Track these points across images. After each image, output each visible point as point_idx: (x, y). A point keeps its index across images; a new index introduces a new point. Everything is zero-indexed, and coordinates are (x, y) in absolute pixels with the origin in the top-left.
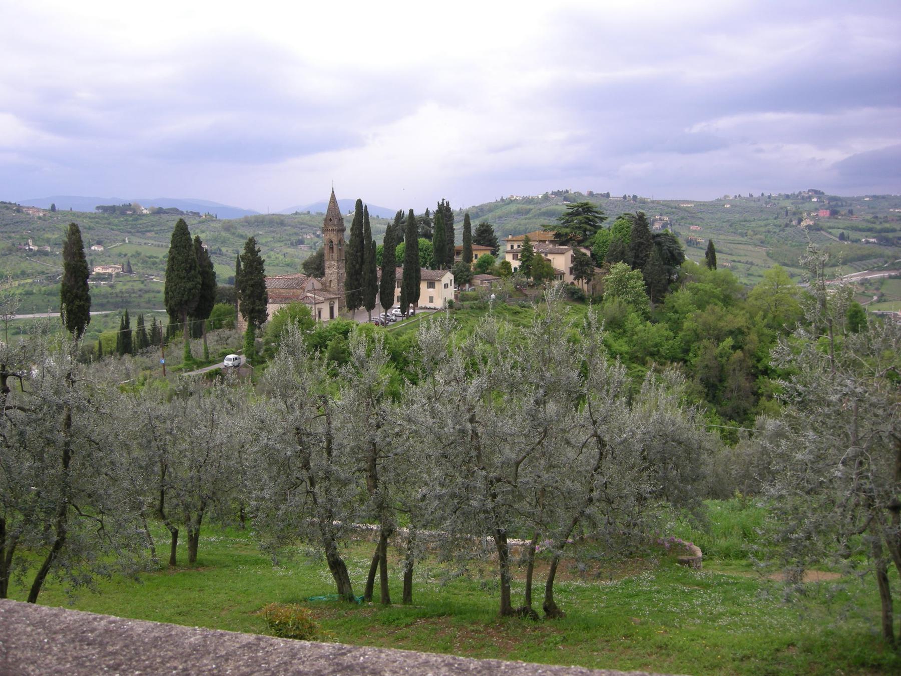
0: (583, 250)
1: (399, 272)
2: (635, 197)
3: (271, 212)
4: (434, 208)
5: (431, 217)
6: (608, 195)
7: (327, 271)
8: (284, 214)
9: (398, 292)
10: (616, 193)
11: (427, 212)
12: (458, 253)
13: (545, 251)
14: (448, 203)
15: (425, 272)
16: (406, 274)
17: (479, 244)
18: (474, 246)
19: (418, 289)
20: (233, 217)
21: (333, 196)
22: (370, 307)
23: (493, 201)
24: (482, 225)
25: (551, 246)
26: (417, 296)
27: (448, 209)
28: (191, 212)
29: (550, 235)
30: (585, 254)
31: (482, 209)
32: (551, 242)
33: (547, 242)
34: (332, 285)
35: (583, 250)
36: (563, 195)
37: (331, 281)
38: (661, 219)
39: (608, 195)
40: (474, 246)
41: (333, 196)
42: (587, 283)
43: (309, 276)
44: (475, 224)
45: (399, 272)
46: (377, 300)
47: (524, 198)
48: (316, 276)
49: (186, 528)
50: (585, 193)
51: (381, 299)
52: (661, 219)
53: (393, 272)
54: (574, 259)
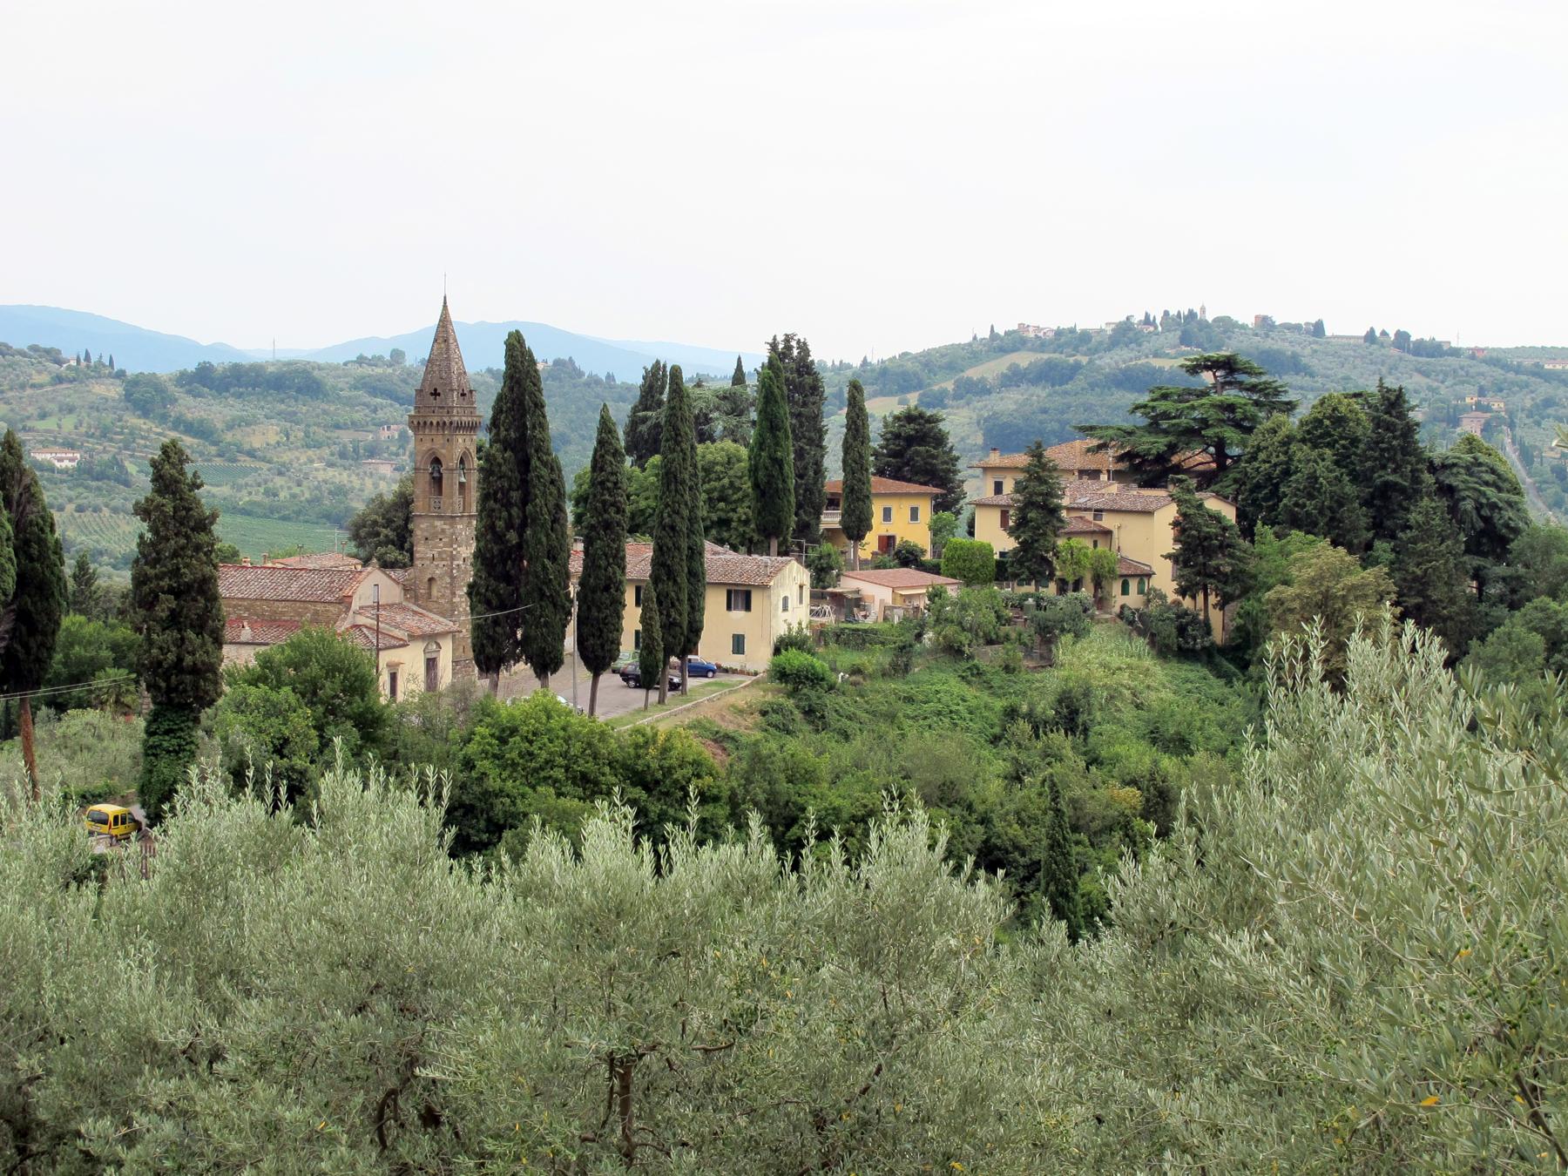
0: (1213, 504)
1: (639, 556)
2: (1402, 337)
3: (285, 357)
4: (756, 358)
5: (752, 381)
6: (1318, 329)
7: (421, 550)
8: (321, 361)
9: (632, 618)
10: (1345, 324)
11: (739, 377)
12: (833, 503)
13: (1094, 504)
14: (804, 348)
15: (719, 559)
16: (662, 566)
17: (897, 475)
18: (877, 483)
19: (696, 609)
20: (165, 369)
21: (444, 322)
22: (546, 664)
23: (966, 339)
24: (909, 418)
25: (1115, 487)
26: (695, 630)
27: (804, 367)
28: (34, 348)
29: (1108, 460)
30: (1217, 518)
31: (926, 365)
32: (1117, 475)
33: (1104, 477)
34: (435, 592)
35: (1213, 504)
36: (1188, 326)
37: (431, 580)
38: (1480, 407)
39: (1318, 329)
40: (877, 483)
41: (444, 322)
42: (1221, 606)
43: (366, 562)
44: (881, 410)
45: (639, 556)
46: (570, 642)
47: (1059, 333)
48: (386, 565)
49: (1167, 736)
50: (1246, 317)
51: (581, 642)
52: (1480, 407)
53: (619, 559)
54: (1182, 527)
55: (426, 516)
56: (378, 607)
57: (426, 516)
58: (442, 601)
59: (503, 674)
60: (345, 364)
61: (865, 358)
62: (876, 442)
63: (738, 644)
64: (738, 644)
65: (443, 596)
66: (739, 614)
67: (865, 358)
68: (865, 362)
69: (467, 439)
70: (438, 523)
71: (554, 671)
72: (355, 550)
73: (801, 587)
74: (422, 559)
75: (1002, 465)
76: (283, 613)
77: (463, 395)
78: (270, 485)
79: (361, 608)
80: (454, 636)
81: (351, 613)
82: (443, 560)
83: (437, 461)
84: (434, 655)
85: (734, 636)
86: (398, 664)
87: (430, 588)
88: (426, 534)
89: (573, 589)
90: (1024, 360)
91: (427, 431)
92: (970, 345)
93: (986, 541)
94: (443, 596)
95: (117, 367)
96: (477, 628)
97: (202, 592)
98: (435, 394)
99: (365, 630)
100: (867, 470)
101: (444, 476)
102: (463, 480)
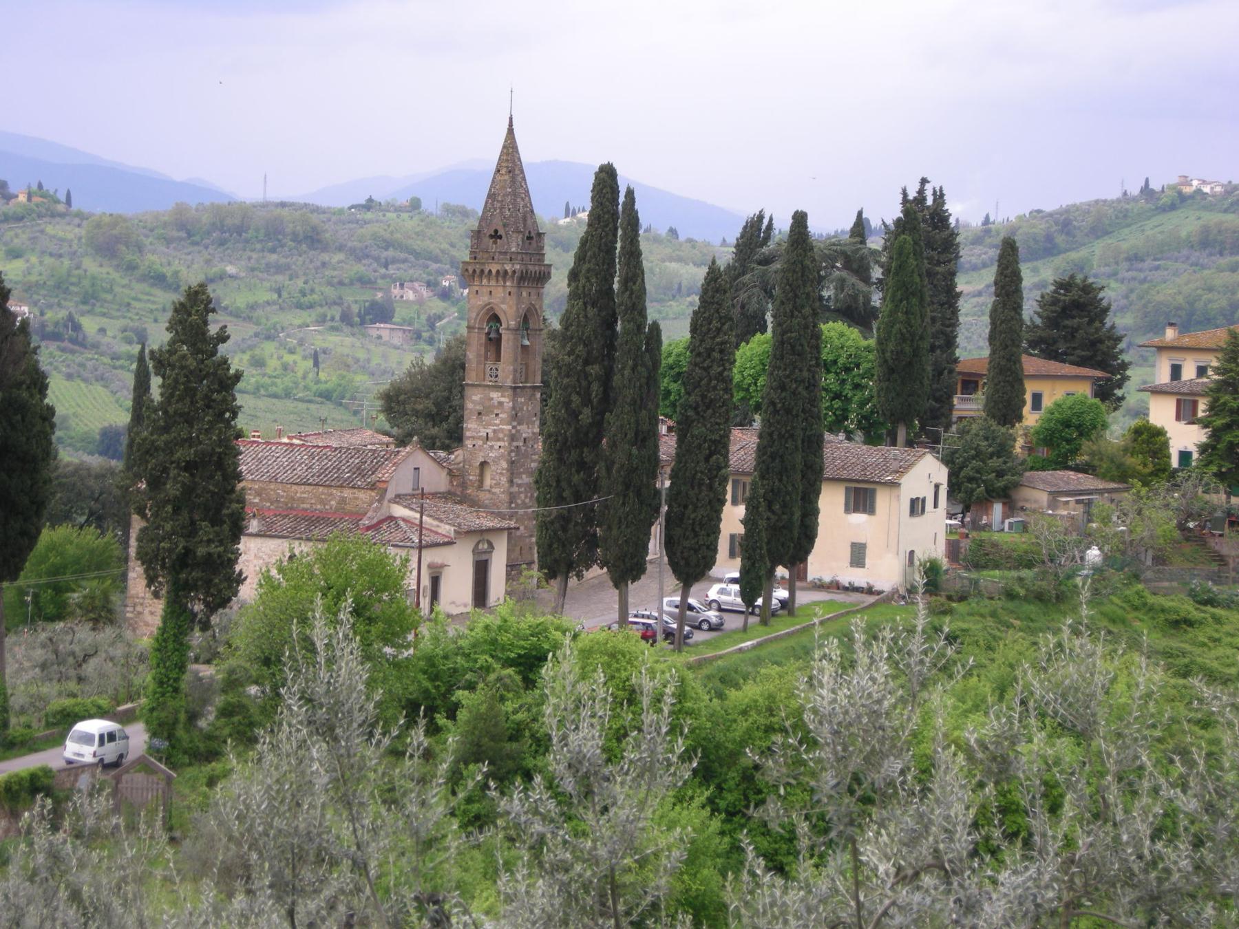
3: (277, 193)
7: (472, 427)
9: (733, 518)
14: (939, 197)
16: (768, 454)
18: (1031, 363)
21: (510, 149)
23: (1114, 194)
27: (939, 217)
34: (488, 482)
37: (483, 464)
40: (1031, 363)
41: (510, 149)
43: (402, 442)
46: (655, 548)
48: (429, 444)
51: (670, 544)
53: (720, 446)
55: (479, 386)
56: (423, 495)
57: (479, 386)
58: (496, 490)
59: (573, 581)
60: (350, 208)
61: (987, 217)
62: (1030, 309)
63: (858, 555)
64: (858, 555)
65: (498, 484)
66: (859, 518)
67: (987, 217)
68: (987, 221)
69: (533, 291)
70: (495, 395)
71: (635, 578)
72: (387, 427)
73: (937, 486)
74: (473, 438)
75: (1179, 344)
76: (303, 500)
77: (529, 238)
78: (257, 352)
79: (398, 496)
80: (509, 534)
81: (385, 502)
82: (499, 440)
83: (495, 318)
84: (484, 557)
85: (854, 545)
86: (443, 566)
87: (482, 474)
88: (479, 408)
89: (665, 484)
90: (1187, 224)
91: (485, 281)
92: (1119, 201)
93: (817, 576)
94: (498, 484)
95: (75, 207)
96: (544, 526)
97: (220, 465)
98: (496, 236)
99: (401, 523)
100: (1019, 346)
101: (504, 338)
102: (527, 342)
